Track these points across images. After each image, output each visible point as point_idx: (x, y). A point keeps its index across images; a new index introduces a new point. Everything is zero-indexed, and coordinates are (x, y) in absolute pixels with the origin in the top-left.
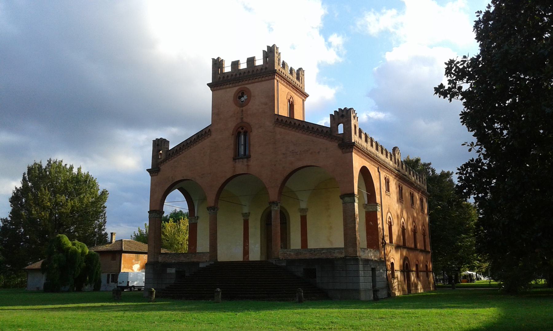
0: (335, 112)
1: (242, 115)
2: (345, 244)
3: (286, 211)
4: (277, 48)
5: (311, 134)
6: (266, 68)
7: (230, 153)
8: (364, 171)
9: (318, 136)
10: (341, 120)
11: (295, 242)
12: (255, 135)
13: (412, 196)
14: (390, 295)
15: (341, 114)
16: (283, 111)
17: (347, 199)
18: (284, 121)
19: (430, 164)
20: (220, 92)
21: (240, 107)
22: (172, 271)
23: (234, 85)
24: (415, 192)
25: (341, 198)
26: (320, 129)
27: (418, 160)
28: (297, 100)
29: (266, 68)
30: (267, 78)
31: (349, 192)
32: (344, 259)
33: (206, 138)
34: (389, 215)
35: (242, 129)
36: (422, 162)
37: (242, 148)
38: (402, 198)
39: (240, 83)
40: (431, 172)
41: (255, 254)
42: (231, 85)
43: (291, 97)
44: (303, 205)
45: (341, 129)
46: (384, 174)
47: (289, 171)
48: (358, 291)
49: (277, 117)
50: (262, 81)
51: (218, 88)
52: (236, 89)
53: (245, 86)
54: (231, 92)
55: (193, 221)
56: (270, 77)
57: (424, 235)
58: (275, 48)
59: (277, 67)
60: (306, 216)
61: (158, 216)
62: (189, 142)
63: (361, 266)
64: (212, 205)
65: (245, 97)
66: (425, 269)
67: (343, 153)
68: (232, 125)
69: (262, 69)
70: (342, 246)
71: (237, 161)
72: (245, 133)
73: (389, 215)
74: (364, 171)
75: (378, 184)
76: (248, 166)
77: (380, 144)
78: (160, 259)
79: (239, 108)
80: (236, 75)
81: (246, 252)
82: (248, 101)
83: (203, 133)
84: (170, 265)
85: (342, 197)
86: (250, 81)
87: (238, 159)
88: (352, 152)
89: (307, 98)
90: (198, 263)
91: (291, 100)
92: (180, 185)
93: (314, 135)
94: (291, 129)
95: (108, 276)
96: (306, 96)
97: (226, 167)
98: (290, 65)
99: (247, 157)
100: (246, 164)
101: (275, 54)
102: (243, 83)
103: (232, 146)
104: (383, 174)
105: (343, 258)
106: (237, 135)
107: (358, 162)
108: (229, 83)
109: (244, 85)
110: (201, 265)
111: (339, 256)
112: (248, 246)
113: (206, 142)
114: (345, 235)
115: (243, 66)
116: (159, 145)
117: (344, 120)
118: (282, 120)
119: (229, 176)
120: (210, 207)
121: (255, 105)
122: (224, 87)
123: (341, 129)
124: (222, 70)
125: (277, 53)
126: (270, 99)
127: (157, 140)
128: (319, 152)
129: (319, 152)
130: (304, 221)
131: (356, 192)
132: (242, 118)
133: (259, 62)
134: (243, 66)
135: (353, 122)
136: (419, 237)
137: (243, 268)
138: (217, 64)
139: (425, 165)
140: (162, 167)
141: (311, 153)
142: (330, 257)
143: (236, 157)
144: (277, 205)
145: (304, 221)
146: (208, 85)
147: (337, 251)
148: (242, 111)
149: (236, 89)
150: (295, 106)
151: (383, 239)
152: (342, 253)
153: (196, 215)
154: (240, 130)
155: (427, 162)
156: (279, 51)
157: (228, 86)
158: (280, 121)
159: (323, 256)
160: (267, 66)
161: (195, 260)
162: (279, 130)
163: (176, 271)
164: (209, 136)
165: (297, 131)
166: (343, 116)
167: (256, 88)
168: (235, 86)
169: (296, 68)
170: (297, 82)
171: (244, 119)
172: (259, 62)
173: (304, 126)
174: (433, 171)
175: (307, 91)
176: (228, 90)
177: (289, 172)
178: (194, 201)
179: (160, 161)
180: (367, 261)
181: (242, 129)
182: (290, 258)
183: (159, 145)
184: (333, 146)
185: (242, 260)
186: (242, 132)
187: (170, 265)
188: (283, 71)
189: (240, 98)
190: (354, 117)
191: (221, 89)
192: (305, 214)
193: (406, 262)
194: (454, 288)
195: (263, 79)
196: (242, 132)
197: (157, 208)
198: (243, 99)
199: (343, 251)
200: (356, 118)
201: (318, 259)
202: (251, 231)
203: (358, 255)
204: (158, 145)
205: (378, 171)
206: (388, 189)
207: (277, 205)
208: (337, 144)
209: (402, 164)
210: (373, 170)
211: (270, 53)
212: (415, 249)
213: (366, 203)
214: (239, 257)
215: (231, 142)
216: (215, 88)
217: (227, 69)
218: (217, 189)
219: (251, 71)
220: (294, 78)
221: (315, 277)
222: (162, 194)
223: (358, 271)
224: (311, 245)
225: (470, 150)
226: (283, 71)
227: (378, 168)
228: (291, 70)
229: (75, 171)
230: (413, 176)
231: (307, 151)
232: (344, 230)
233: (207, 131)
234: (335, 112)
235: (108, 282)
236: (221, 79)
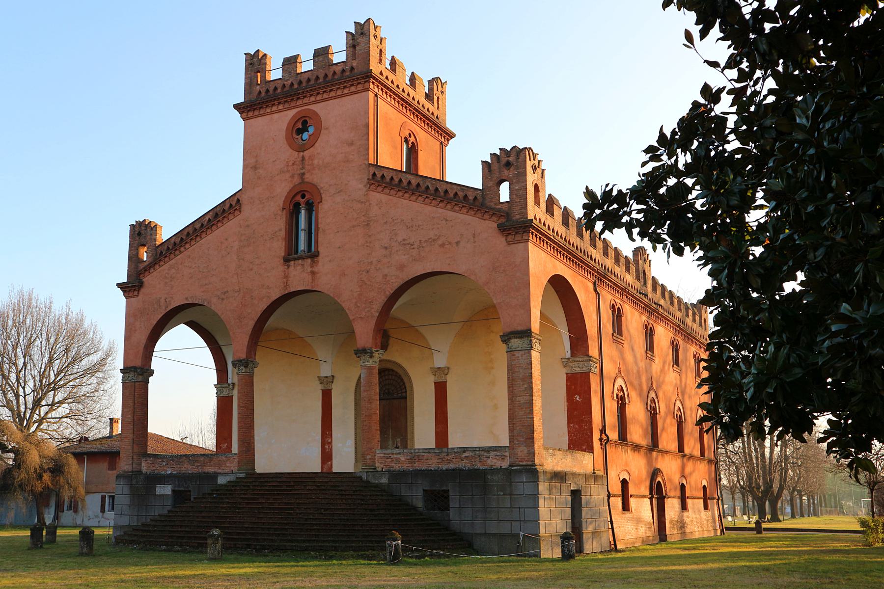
0: (493, 155)
1: (303, 168)
2: (511, 440)
3: (407, 374)
4: (376, 27)
5: (442, 205)
6: (352, 69)
7: (279, 247)
8: (558, 284)
9: (456, 208)
10: (506, 173)
11: (423, 434)
12: (327, 211)
13: (650, 333)
15: (504, 160)
16: (391, 157)
17: (515, 343)
18: (388, 179)
20: (260, 122)
23: (287, 105)
25: (504, 341)
26: (461, 194)
28: (425, 139)
29: (352, 69)
31: (520, 328)
32: (509, 473)
33: (231, 217)
34: (620, 382)
35: (303, 196)
37: (302, 236)
38: (620, 332)
39: (299, 102)
41: (345, 461)
42: (281, 107)
44: (440, 361)
45: (504, 193)
46: (609, 297)
47: (396, 284)
48: (534, 539)
49: (372, 170)
51: (256, 113)
52: (291, 113)
54: (281, 120)
55: (225, 394)
56: (360, 87)
58: (372, 27)
59: (375, 67)
60: (446, 382)
61: (140, 378)
63: (543, 487)
64: (243, 356)
65: (311, 130)
67: (509, 243)
68: (282, 189)
70: (506, 443)
71: (292, 263)
72: (310, 207)
73: (620, 382)
74: (558, 284)
76: (313, 273)
77: (677, 293)
78: (145, 467)
80: (292, 84)
81: (327, 456)
82: (315, 138)
83: (227, 207)
84: (162, 479)
85: (506, 338)
86: (319, 97)
87: (295, 259)
88: (527, 241)
89: (451, 141)
90: (215, 476)
91: (412, 139)
92: (190, 314)
93: (449, 206)
94: (400, 194)
95: (103, 498)
96: (450, 136)
97: (271, 278)
98: (409, 66)
99: (313, 255)
100: (309, 269)
101: (372, 38)
102: (306, 100)
104: (608, 297)
105: (506, 469)
107: (541, 264)
110: (221, 480)
112: (331, 443)
113: (232, 225)
114: (512, 418)
115: (307, 66)
117: (512, 172)
119: (276, 295)
120: (240, 361)
121: (329, 145)
122: (268, 110)
123: (504, 193)
124: (264, 77)
125: (375, 37)
126: (362, 132)
127: (140, 224)
128: (458, 243)
129: (458, 243)
130: (441, 390)
131: (535, 326)
132: (303, 174)
133: (339, 57)
135: (531, 178)
137: (324, 484)
138: (255, 63)
140: (147, 279)
141: (442, 245)
142: (479, 466)
143: (291, 255)
144: (371, 357)
145: (441, 390)
146: (236, 107)
147: (492, 454)
148: (303, 158)
149: (291, 113)
150: (420, 154)
151: (603, 430)
152: (503, 458)
153: (230, 381)
154: (298, 198)
156: (382, 34)
157: (274, 108)
158: (381, 179)
159: (465, 465)
161: (211, 470)
162: (378, 197)
163: (173, 491)
164: (237, 213)
165: (414, 198)
166: (508, 164)
167: (332, 111)
168: (290, 109)
169: (425, 77)
170: (428, 105)
171: (307, 176)
172: (339, 57)
173: (427, 188)
175: (450, 125)
176: (276, 116)
177: (396, 286)
178: (224, 349)
179: (141, 266)
180: (559, 476)
181: (303, 196)
182: (397, 467)
184: (487, 227)
186: (302, 203)
187: (162, 479)
188: (391, 76)
189: (300, 132)
190: (534, 168)
191: (262, 115)
192: (443, 380)
194: (759, 532)
196: (302, 203)
197: (138, 363)
198: (305, 136)
199: (507, 454)
200: (539, 171)
201: (454, 470)
202: (336, 413)
203: (537, 461)
204: (139, 234)
205: (595, 290)
206: (618, 329)
207: (371, 357)
208: (496, 225)
209: (687, 309)
210: (582, 287)
211: (361, 36)
213: (568, 355)
214: (314, 465)
215: (280, 224)
216: (250, 114)
217: (275, 73)
218: (252, 324)
219: (321, 76)
220: (418, 95)
221: (447, 508)
222: (148, 332)
223: (535, 497)
224: (455, 441)
226: (391, 76)
227: (595, 284)
228: (413, 79)
230: (680, 310)
231: (434, 240)
232: (510, 410)
233: (234, 204)
234: (493, 155)
235: (103, 510)
236: (263, 94)
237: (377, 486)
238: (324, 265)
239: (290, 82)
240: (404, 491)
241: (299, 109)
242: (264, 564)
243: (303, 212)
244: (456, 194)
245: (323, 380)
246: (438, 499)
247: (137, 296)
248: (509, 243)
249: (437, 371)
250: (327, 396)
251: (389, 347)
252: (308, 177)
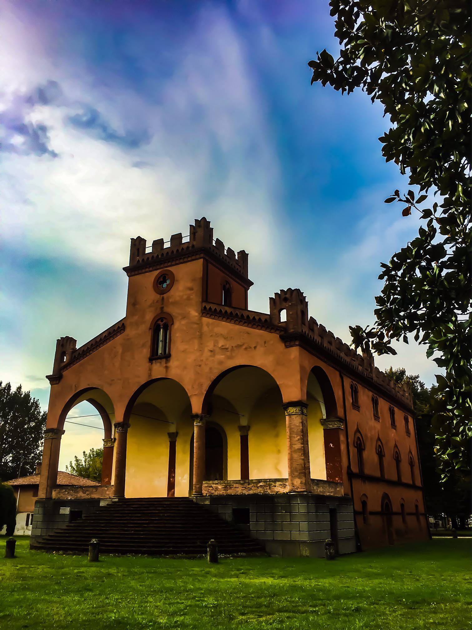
6: (193, 246)
7: (146, 352)
10: (284, 304)
11: (234, 472)
15: (283, 296)
18: (213, 310)
19: (418, 377)
21: (160, 294)
22: (66, 511)
24: (409, 417)
26: (257, 318)
27: (403, 372)
29: (193, 246)
36: (408, 374)
39: (162, 266)
40: (419, 387)
41: (182, 490)
43: (227, 282)
52: (156, 273)
54: (151, 276)
57: (412, 464)
62: (98, 340)
66: (414, 511)
69: (188, 247)
71: (154, 361)
72: (167, 328)
75: (340, 393)
79: (159, 296)
80: (158, 256)
81: (171, 486)
84: (65, 503)
90: (99, 500)
95: (28, 516)
97: (140, 370)
99: (167, 357)
100: (165, 365)
102: (166, 265)
103: (149, 343)
106: (155, 329)
110: (102, 504)
111: (282, 490)
113: (119, 339)
116: (65, 345)
119: (143, 381)
128: (255, 347)
129: (255, 347)
136: (405, 467)
139: (411, 378)
141: (246, 349)
143: (154, 357)
147: (278, 483)
148: (163, 298)
149: (156, 273)
153: (113, 437)
155: (414, 375)
160: (195, 243)
163: (71, 511)
166: (286, 300)
174: (422, 385)
179: (63, 365)
183: (65, 345)
185: (166, 496)
187: (65, 503)
193: (386, 501)
198: (165, 285)
204: (62, 345)
212: (399, 483)
213: (325, 417)
214: (164, 494)
215: (148, 339)
216: (133, 273)
225: (406, 212)
229: (13, 390)
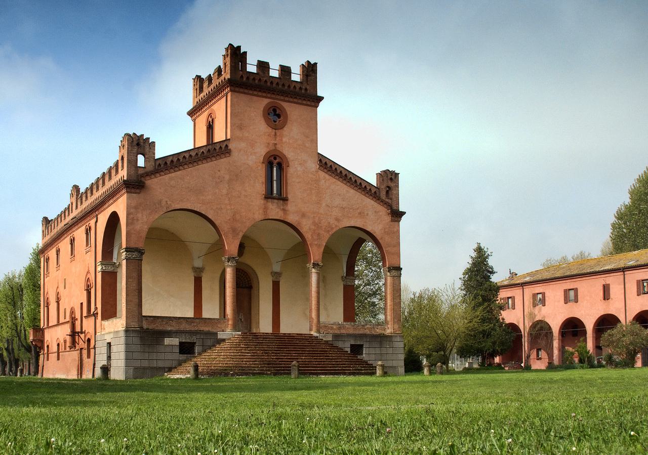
14: (572, 362)
26: (368, 188)
30: (309, 103)
50: (242, 93)
53: (280, 102)
55: (110, 269)
84: (169, 334)
102: (279, 97)
108: (311, 100)
109: (278, 99)
118: (331, 166)
133: (296, 77)
134: (274, 73)
140: (153, 183)
143: (269, 196)
153: (115, 260)
162: (322, 174)
195: (305, 102)
213: (345, 275)
233: (223, 147)
237: (327, 342)
238: (291, 207)
239: (265, 79)
240: (340, 344)
241: (272, 100)
242: (523, 339)
243: (275, 169)
244: (365, 187)
245: (274, 274)
246: (357, 349)
247: (139, 193)
248: (392, 221)
249: (274, 274)
250: (198, 282)
251: (244, 255)
252: (278, 147)
